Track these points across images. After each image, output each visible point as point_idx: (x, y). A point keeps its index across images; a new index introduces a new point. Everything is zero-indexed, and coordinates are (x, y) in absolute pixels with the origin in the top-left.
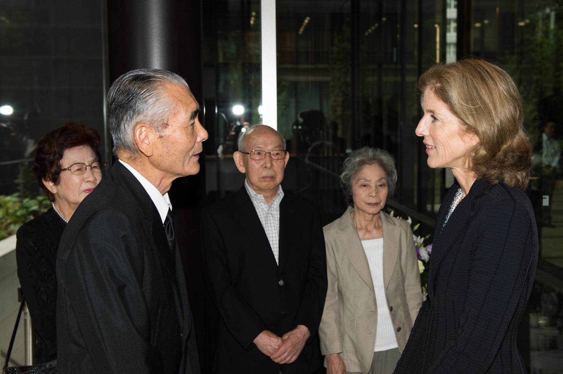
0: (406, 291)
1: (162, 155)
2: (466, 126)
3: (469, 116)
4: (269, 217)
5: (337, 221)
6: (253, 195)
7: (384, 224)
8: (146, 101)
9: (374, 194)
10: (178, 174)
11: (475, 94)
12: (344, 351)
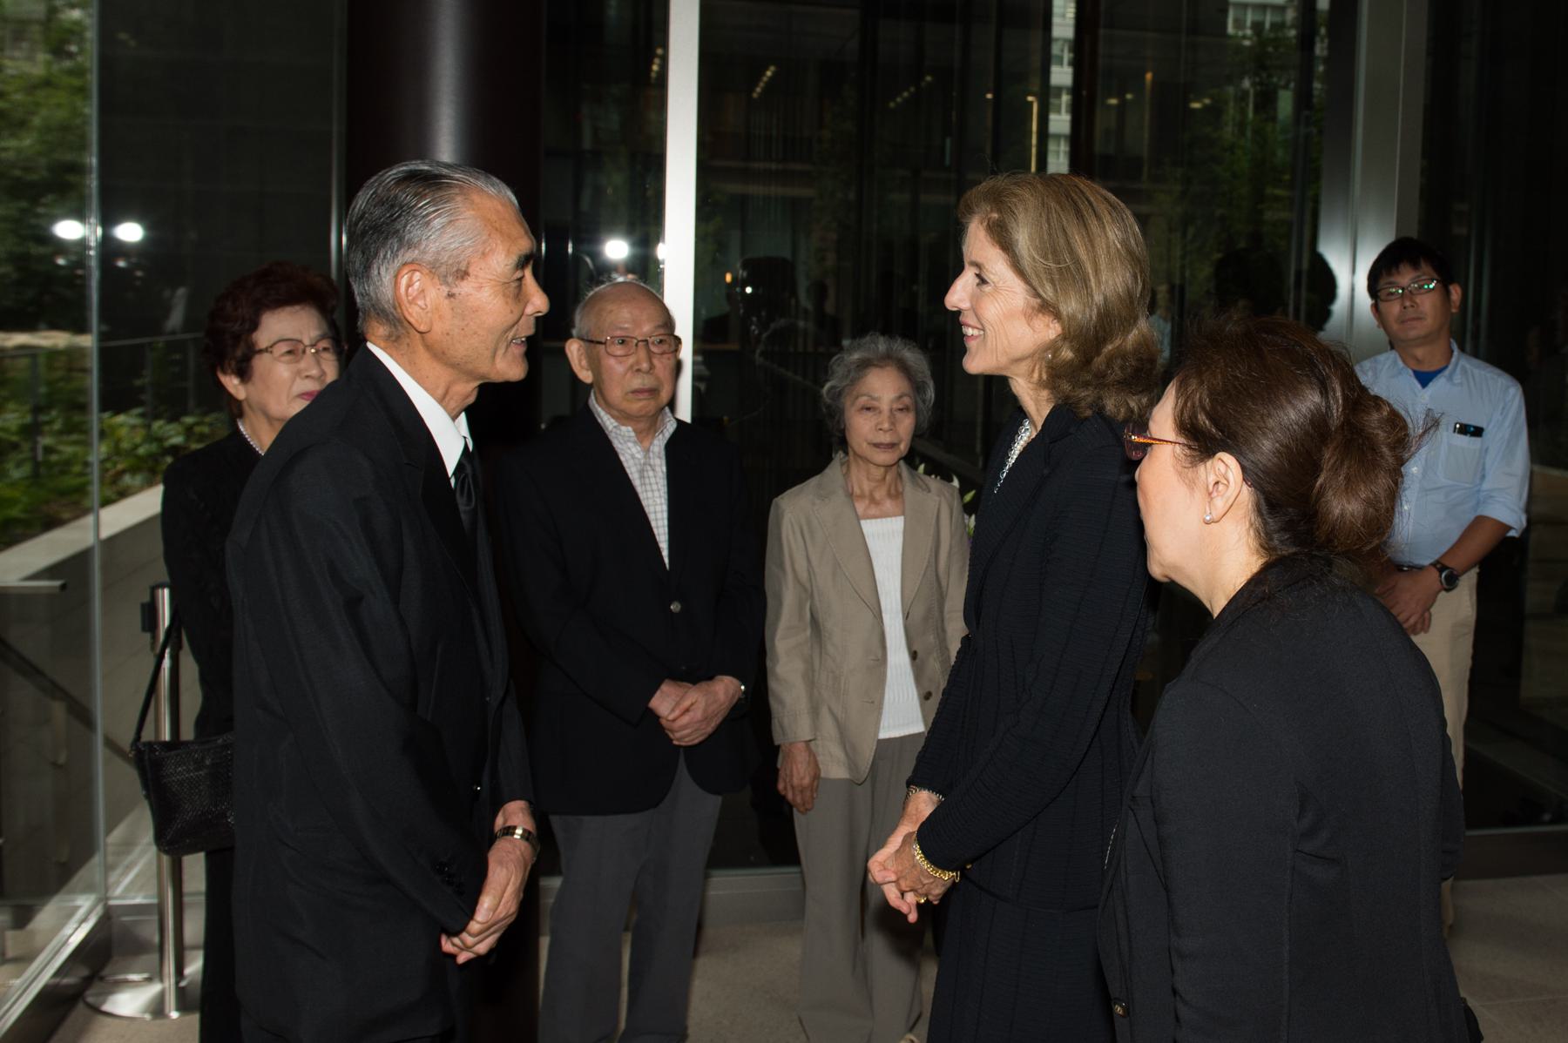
0: (946, 623)
1: (451, 333)
2: (1039, 301)
3: (1045, 282)
4: (647, 471)
5: (814, 481)
6: (610, 428)
7: (909, 489)
8: (428, 223)
9: (886, 426)
10: (482, 377)
11: (1062, 241)
12: (819, 738)
